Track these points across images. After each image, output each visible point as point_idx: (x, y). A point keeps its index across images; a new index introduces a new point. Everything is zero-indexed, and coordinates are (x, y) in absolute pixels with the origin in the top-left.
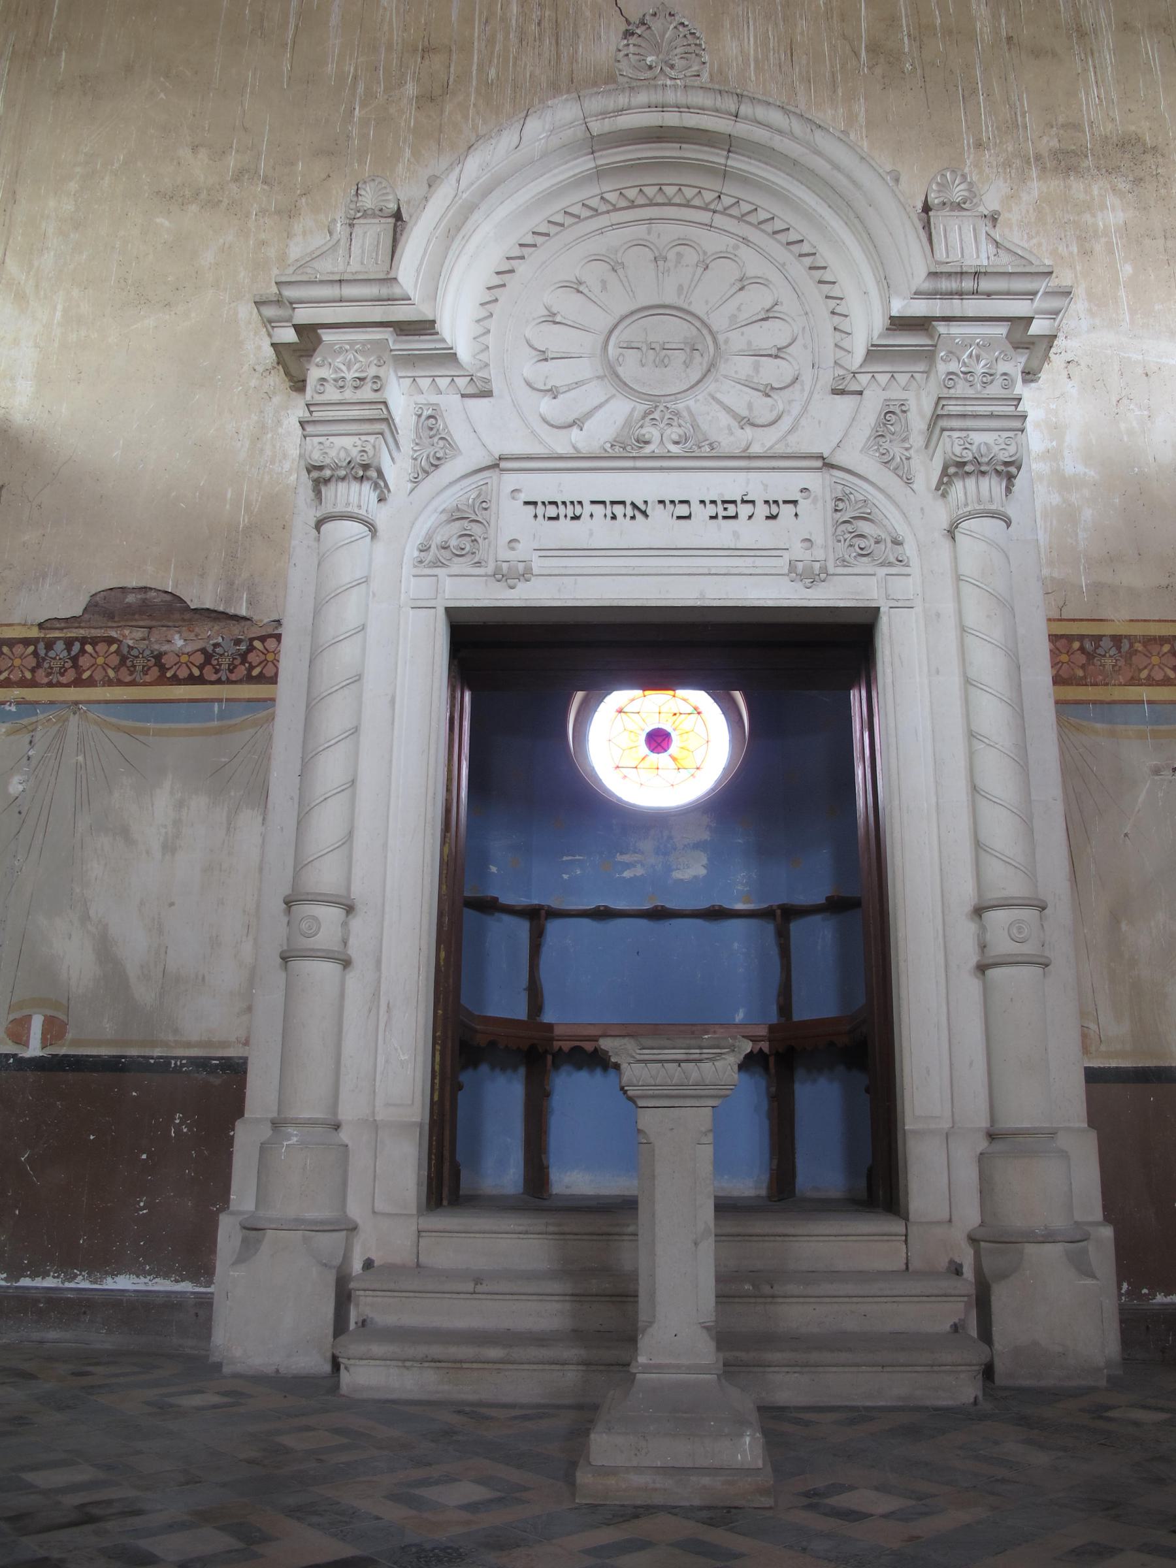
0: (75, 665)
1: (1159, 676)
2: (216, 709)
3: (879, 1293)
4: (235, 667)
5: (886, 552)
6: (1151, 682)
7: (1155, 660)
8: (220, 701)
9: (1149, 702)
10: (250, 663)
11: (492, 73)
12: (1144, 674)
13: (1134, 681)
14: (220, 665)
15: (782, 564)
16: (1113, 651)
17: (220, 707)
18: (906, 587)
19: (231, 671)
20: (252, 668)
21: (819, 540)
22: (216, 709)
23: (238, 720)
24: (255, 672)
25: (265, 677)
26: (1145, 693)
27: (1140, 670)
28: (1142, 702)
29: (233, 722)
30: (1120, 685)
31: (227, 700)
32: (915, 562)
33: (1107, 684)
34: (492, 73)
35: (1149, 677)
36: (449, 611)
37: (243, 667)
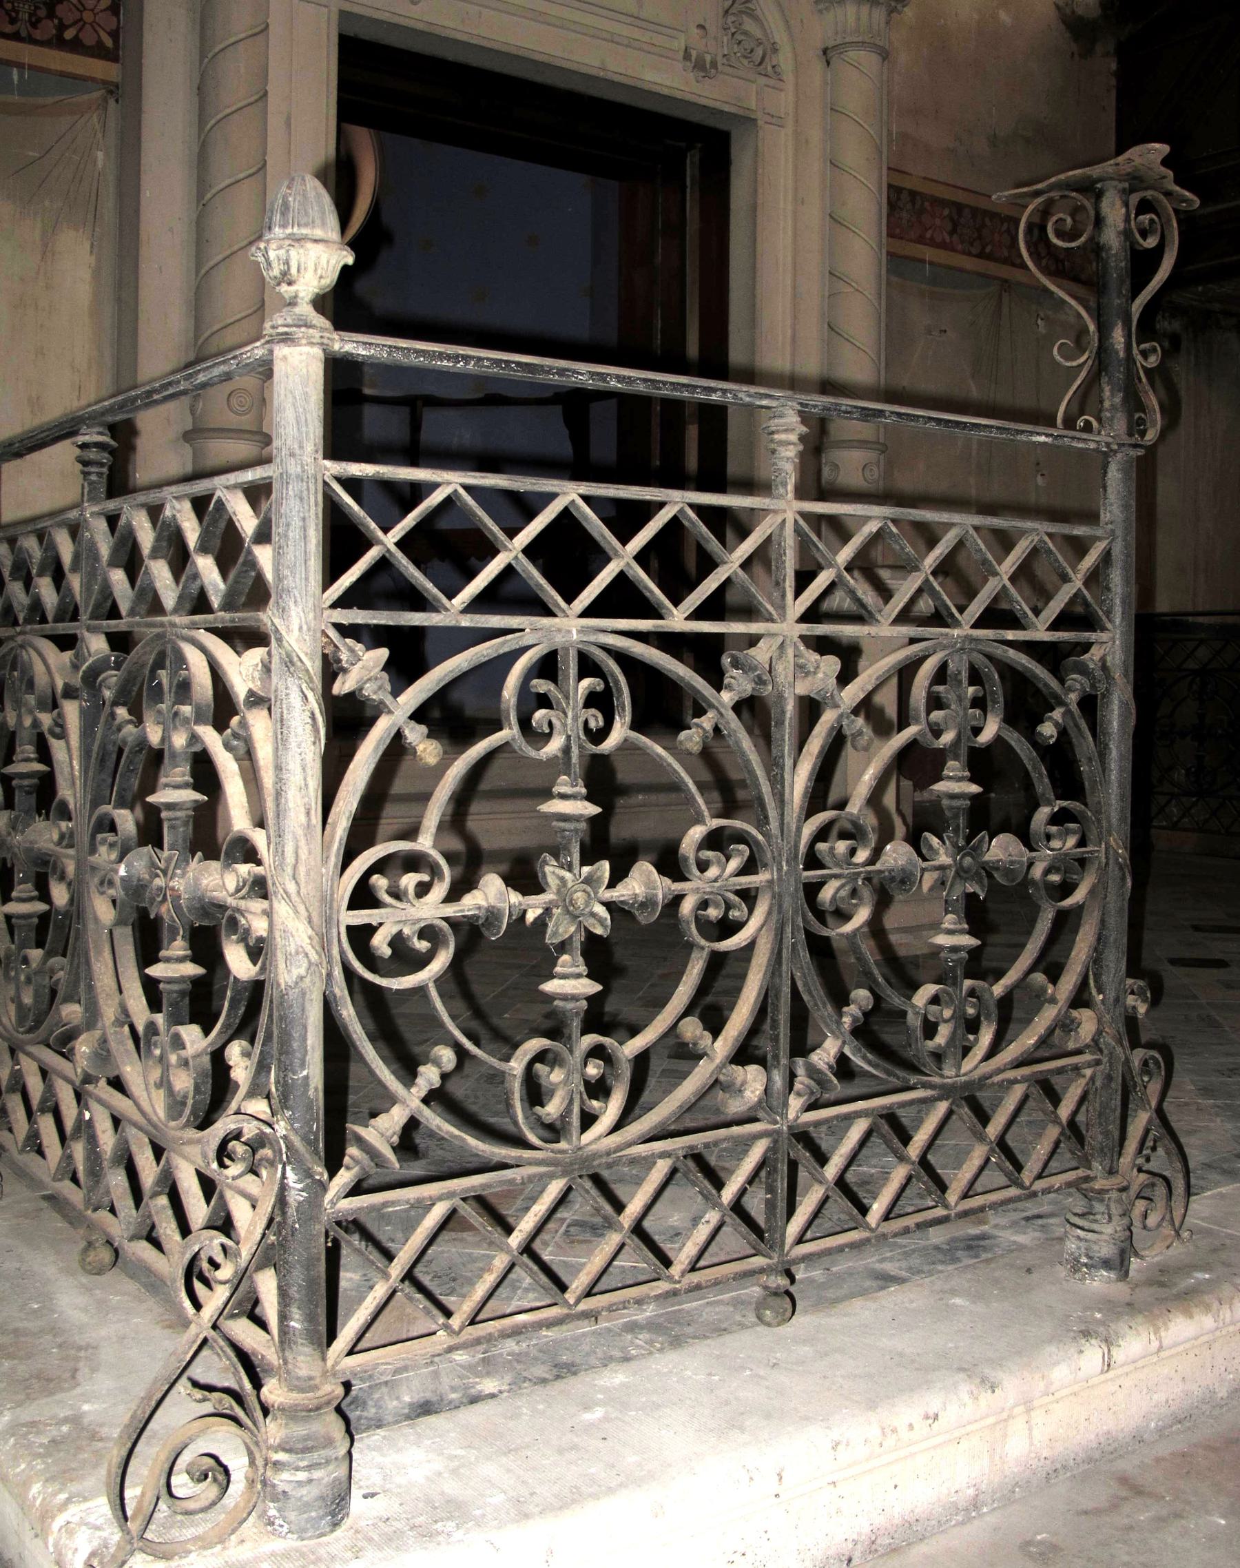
0: (980, 237)
1: (939, 239)
2: (16, 77)
3: (728, 1258)
4: (39, 20)
5: (760, 58)
6: (932, 243)
7: (938, 222)
8: (20, 66)
9: (931, 263)
10: (60, 20)
11: (600, 1396)
12: (928, 235)
13: (921, 240)
14: (17, 12)
15: (679, 44)
16: (909, 206)
17: (21, 76)
18: (784, 101)
19: (34, 25)
20: (62, 27)
21: (712, 29)
22: (16, 77)
23: (50, 100)
24: (69, 34)
25: (83, 46)
26: (929, 253)
27: (927, 230)
28: (923, 261)
29: (41, 101)
30: (911, 241)
31: (31, 67)
32: (789, 77)
33: (901, 238)
34: (600, 1396)
35: (932, 239)
36: (344, 15)
37: (50, 24)
